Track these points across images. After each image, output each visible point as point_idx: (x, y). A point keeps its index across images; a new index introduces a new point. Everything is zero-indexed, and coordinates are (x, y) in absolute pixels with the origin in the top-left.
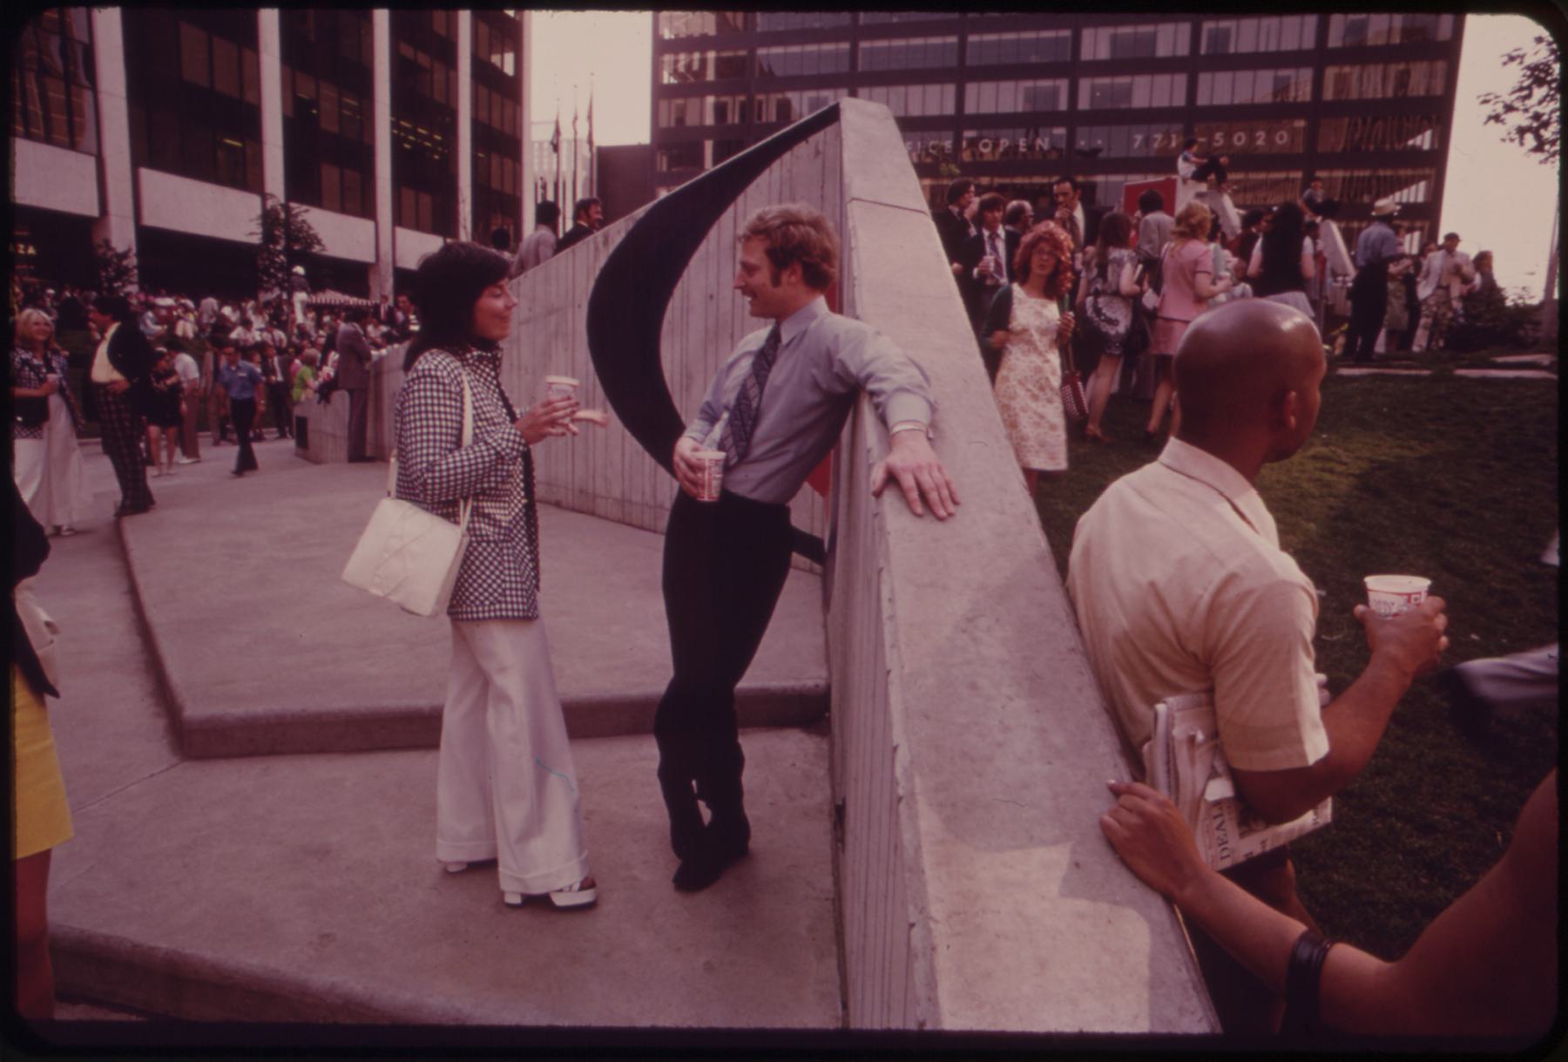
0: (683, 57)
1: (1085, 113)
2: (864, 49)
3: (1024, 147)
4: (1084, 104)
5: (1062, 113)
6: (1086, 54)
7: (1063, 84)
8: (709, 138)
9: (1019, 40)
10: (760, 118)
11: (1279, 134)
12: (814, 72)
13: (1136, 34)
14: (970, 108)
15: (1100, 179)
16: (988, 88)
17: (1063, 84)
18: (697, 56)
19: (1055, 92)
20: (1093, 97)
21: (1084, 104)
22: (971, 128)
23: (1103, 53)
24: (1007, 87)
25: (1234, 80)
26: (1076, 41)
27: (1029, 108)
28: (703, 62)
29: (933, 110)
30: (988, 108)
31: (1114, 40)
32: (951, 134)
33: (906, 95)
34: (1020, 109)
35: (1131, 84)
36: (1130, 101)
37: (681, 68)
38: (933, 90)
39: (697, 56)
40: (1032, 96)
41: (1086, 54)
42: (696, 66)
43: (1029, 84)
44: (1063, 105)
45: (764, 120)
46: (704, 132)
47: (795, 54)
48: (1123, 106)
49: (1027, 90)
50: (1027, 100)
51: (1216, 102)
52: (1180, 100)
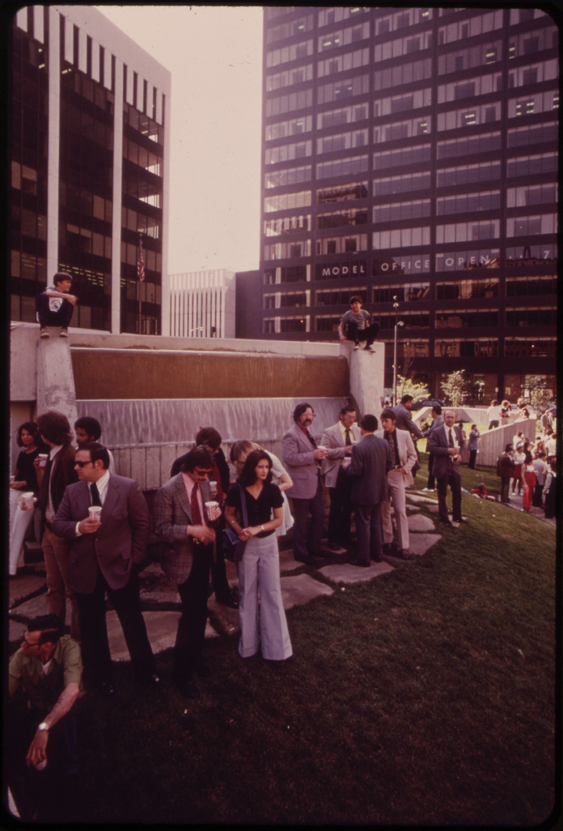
0: (287, 220)
1: (511, 239)
2: (440, 202)
3: (355, 271)
4: (510, 234)
5: (497, 240)
6: (510, 204)
7: (496, 223)
8: (308, 263)
9: (479, 197)
10: (319, 253)
11: (383, 265)
12: (409, 217)
13: (541, 189)
14: (439, 240)
15: (407, 286)
16: (450, 228)
17: (496, 223)
18: (301, 218)
19: (492, 228)
20: (515, 231)
21: (510, 234)
22: (440, 252)
23: (521, 202)
24: (462, 227)
25: (456, 228)
26: (503, 197)
27: (476, 238)
28: (305, 221)
29: (417, 243)
30: (450, 239)
31: (528, 195)
32: (428, 256)
33: (401, 234)
34: (470, 239)
35: (541, 220)
36: (540, 231)
37: (287, 227)
38: (417, 231)
39: (301, 218)
40: (476, 231)
41: (510, 204)
42: (301, 225)
43: (475, 224)
44: (497, 235)
45: (321, 254)
46: (307, 260)
47: (396, 208)
48: (537, 233)
49: (474, 228)
50: (474, 233)
51: (447, 241)
52: (427, 241)
